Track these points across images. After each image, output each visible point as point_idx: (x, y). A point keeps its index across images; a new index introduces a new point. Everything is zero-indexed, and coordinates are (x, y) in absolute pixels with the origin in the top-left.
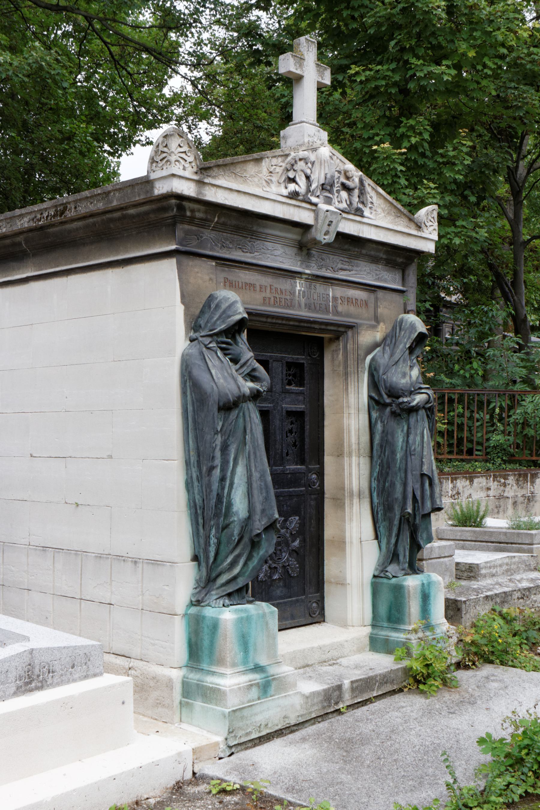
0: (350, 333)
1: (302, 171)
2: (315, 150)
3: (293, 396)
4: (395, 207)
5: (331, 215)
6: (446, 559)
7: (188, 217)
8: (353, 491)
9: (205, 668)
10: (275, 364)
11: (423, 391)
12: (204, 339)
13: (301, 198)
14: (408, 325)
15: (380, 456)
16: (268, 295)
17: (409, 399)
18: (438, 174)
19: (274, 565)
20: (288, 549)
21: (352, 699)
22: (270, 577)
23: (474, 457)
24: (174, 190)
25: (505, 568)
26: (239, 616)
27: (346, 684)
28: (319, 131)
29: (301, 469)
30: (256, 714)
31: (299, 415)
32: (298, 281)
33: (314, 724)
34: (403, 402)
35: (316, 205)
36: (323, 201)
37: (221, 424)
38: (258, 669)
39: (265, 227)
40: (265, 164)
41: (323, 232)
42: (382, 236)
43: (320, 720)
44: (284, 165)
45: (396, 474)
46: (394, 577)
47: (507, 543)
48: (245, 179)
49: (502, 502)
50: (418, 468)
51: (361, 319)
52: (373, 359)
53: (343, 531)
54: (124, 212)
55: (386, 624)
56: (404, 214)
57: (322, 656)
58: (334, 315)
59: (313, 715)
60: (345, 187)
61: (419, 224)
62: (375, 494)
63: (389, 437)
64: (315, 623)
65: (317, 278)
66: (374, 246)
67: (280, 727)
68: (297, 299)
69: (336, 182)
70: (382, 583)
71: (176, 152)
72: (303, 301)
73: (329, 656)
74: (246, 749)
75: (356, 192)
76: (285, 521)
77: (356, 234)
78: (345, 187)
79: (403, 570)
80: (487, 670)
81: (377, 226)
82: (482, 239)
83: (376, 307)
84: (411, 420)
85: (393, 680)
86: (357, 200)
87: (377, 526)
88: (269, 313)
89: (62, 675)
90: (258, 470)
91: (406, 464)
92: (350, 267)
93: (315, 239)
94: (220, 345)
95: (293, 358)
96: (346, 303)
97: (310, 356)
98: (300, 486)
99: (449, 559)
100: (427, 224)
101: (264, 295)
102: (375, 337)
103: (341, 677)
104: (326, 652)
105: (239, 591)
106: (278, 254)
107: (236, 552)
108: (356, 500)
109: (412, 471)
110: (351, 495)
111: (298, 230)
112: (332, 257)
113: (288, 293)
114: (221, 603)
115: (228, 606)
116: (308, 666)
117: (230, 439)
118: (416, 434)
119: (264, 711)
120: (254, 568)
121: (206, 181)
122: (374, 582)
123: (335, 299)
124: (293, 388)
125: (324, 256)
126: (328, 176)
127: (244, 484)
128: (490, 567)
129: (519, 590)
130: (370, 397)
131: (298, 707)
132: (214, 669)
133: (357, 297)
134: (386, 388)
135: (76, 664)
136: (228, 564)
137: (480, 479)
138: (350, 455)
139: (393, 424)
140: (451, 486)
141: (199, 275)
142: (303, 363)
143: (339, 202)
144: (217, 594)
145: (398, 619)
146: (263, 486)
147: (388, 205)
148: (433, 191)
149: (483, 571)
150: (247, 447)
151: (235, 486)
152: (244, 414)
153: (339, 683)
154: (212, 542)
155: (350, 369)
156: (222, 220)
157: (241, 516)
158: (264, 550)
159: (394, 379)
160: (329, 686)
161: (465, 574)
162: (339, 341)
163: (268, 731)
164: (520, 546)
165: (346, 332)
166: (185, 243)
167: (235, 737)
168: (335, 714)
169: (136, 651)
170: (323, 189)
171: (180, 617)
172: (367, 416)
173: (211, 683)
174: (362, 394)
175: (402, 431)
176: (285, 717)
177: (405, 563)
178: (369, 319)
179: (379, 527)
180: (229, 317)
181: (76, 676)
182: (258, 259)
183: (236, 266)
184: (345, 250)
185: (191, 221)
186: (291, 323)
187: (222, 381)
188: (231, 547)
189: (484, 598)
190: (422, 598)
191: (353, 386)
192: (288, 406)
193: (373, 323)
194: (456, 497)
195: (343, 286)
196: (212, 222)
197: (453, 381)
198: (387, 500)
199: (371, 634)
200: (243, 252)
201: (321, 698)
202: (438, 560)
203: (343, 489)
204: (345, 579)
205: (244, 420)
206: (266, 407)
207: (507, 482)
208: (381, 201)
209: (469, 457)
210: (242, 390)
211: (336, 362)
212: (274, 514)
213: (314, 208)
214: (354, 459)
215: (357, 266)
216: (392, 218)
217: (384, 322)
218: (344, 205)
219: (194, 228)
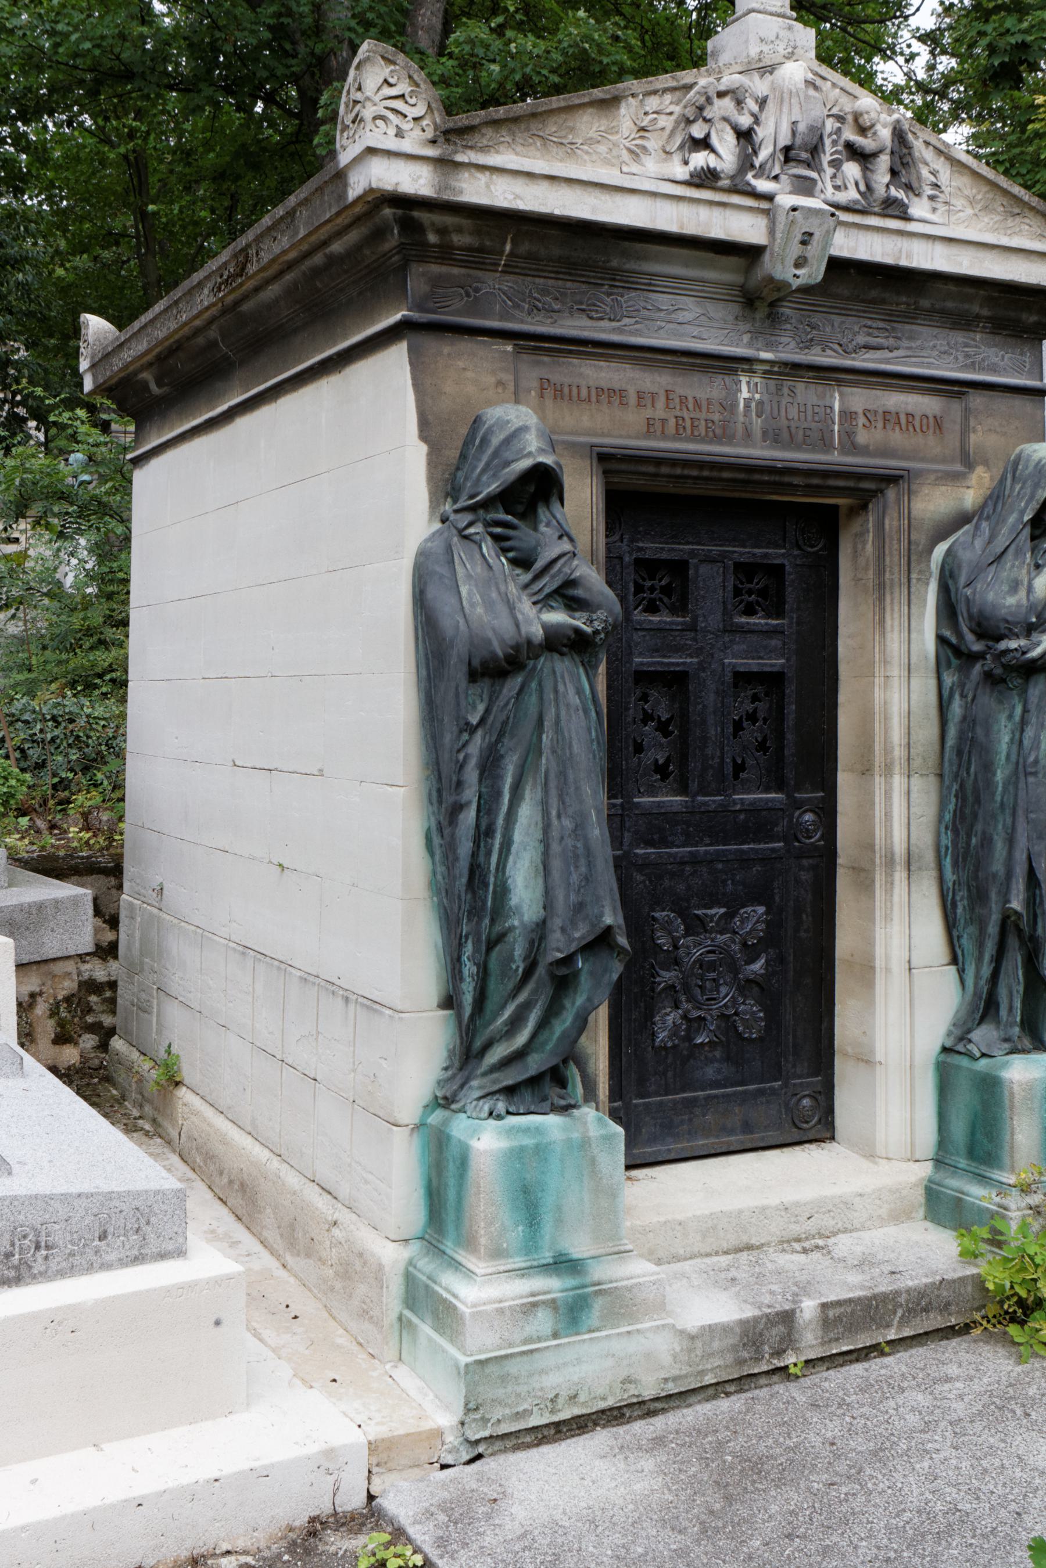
0: (891, 493)
1: (725, 119)
2: (767, 70)
3: (754, 638)
4: (1006, 192)
5: (806, 218)
7: (434, 246)
8: (893, 854)
9: (449, 1251)
10: (704, 569)
12: (459, 516)
13: (724, 183)
14: (1031, 468)
15: (956, 775)
16: (660, 411)
17: (1023, 642)
19: (695, 1014)
20: (735, 977)
21: (823, 1344)
24: (374, 186)
26: (515, 1143)
27: (809, 1308)
28: (790, 28)
30: (543, 1372)
32: (744, 380)
33: (715, 1397)
34: (1008, 651)
35: (769, 198)
36: (788, 188)
37: (481, 708)
38: (564, 1264)
39: (645, 258)
40: (627, 114)
41: (790, 261)
43: (731, 1388)
44: (677, 109)
45: (994, 817)
46: (984, 1055)
48: (570, 150)
51: (923, 460)
52: (949, 552)
53: (870, 942)
54: (327, 251)
55: (963, 1163)
56: (1032, 209)
57: (793, 1226)
58: (843, 451)
59: (709, 1379)
60: (854, 152)
62: (948, 862)
63: (979, 731)
64: (810, 1142)
65: (795, 369)
66: (952, 287)
67: (610, 1402)
68: (741, 419)
69: (828, 142)
70: (958, 1067)
71: (377, 99)
72: (757, 424)
73: (811, 1226)
74: (516, 1448)
75: (884, 161)
76: (730, 916)
77: (889, 260)
78: (854, 152)
79: (1006, 1040)
83: (965, 431)
84: (1031, 691)
86: (887, 178)
87: (955, 933)
89: (72, 1254)
90: (570, 811)
91: (1016, 795)
92: (891, 341)
93: (771, 279)
94: (491, 529)
96: (880, 425)
97: (800, 548)
98: (772, 839)
101: (649, 413)
102: (961, 500)
103: (805, 1289)
105: (534, 1082)
106: (693, 322)
107: (522, 998)
108: (900, 875)
109: (1027, 811)
110: (890, 862)
111: (733, 260)
112: (837, 320)
114: (486, 1108)
115: (499, 1117)
116: (749, 1248)
117: (506, 741)
119: (565, 1364)
120: (564, 1035)
121: (460, 158)
122: (944, 1062)
123: (848, 415)
124: (757, 621)
125: (816, 319)
126: (802, 127)
127: (537, 844)
130: (941, 639)
131: (666, 1359)
132: (461, 1256)
133: (910, 409)
134: (971, 617)
135: (111, 1230)
136: (505, 1023)
139: (987, 700)
141: (469, 374)
142: (783, 566)
143: (837, 188)
144: (480, 1088)
145: (990, 1155)
146: (581, 851)
147: (985, 188)
150: (544, 761)
151: (514, 848)
152: (540, 684)
154: (466, 972)
155: (894, 574)
156: (525, 248)
157: (526, 918)
158: (584, 997)
159: (991, 596)
160: (757, 1313)
163: (577, 1411)
165: (882, 491)
166: (431, 305)
167: (485, 1420)
168: (775, 1378)
169: (344, 1191)
170: (787, 160)
171: (406, 1131)
172: (932, 683)
173: (446, 1289)
174: (921, 632)
175: (1010, 717)
176: (628, 1380)
177: (1012, 1025)
178: (944, 460)
179: (959, 937)
180: (507, 463)
181: (112, 1257)
182: (631, 333)
183: (571, 352)
184: (873, 301)
185: (445, 253)
186: (726, 475)
187: (480, 610)
188: (510, 986)
191: (896, 615)
192: (739, 659)
193: (958, 467)
196: (501, 253)
199: (930, 1181)
200: (591, 318)
201: (731, 1341)
203: (872, 847)
204: (872, 1051)
205: (541, 699)
206: (678, 664)
208: (964, 181)
210: (523, 630)
211: (862, 561)
212: (602, 915)
213: (764, 205)
214: (898, 781)
215: (911, 338)
216: (997, 218)
218: (851, 195)
219: (456, 271)
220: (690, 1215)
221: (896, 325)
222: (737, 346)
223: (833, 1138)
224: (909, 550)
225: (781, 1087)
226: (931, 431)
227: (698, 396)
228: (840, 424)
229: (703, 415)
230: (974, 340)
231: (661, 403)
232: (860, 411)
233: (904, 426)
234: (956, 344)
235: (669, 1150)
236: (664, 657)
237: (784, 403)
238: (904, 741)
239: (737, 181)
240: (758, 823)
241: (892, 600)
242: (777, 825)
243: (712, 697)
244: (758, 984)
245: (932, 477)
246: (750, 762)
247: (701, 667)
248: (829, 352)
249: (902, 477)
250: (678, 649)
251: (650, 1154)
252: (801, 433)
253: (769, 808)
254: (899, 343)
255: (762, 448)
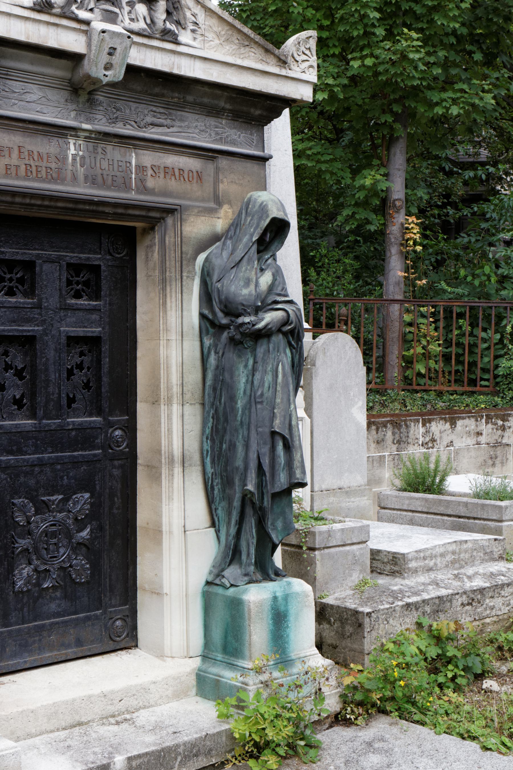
0: (170, 220)
3: (81, 314)
4: (239, 31)
5: (111, 38)
6: (355, 547)
8: (173, 456)
10: (46, 267)
11: (279, 306)
13: (57, 11)
14: (257, 207)
15: (213, 404)
16: (14, 160)
17: (253, 318)
18: (428, 22)
19: (42, 568)
20: (70, 542)
22: (38, 584)
23: (478, 388)
25: (449, 558)
29: (94, 421)
31: (93, 342)
32: (72, 142)
34: (243, 324)
35: (87, 23)
36: (100, 18)
42: (215, 74)
45: (237, 430)
46: (232, 585)
47: (469, 518)
49: (499, 451)
50: (267, 423)
51: (190, 199)
52: (207, 260)
53: (159, 515)
56: (256, 43)
57: (109, 707)
58: (138, 191)
61: (283, 58)
62: (208, 460)
63: (227, 375)
64: (121, 649)
65: (106, 136)
66: (206, 89)
68: (70, 168)
70: (217, 594)
72: (81, 171)
73: (121, 706)
76: (65, 500)
77: (166, 69)
79: (246, 575)
80: (381, 727)
81: (205, 59)
82: (490, 107)
83: (216, 182)
84: (258, 350)
85: (210, 750)
86: (164, 16)
87: (213, 507)
88: (47, 193)
92: (169, 122)
95: (80, 258)
96: (162, 175)
97: (111, 255)
98: (94, 448)
99: (361, 546)
100: (298, 58)
102: (214, 226)
104: (116, 702)
108: (178, 470)
109: (257, 427)
110: (171, 461)
112: (134, 105)
113: (53, 159)
116: (80, 724)
118: (265, 372)
122: (207, 591)
123: (141, 168)
124: (83, 302)
125: (120, 104)
128: (425, 558)
129: (465, 593)
130: (202, 316)
133: (181, 166)
134: (221, 301)
137: (467, 421)
138: (169, 402)
139: (231, 355)
140: (422, 430)
142: (100, 266)
145: (236, 649)
147: (227, 28)
148: (415, 43)
149: (413, 565)
153: (105, 762)
155: (172, 273)
159: (233, 288)
161: (388, 568)
162: (154, 232)
164: (485, 522)
165: (163, 219)
172: (197, 344)
174: (190, 311)
175: (246, 366)
177: (249, 565)
184: (157, 95)
189: (402, 606)
190: (273, 619)
191: (174, 300)
193: (212, 205)
194: (430, 445)
195: (155, 150)
197: (459, 290)
198: (226, 470)
199: (199, 670)
202: (341, 549)
203: (159, 452)
204: (161, 587)
206: (29, 331)
207: (507, 424)
208: (213, 22)
209: (471, 389)
211: (151, 264)
213: (84, 27)
214: (176, 408)
215: (181, 120)
216: (235, 47)
217: (230, 203)
218: (141, 25)
220: (39, 705)
221: (171, 111)
222: (67, 119)
223: (136, 646)
224: (182, 257)
225: (102, 614)
226: (195, 180)
227: (41, 151)
228: (136, 174)
229: (44, 164)
230: (221, 124)
231: (15, 154)
232: (149, 166)
233: (177, 177)
234: (210, 126)
235: (25, 662)
236: (19, 326)
237: (98, 158)
238: (179, 382)
239: (65, 10)
240: (85, 437)
241: (171, 289)
242: (97, 438)
243: (52, 353)
244: (85, 545)
245: (196, 211)
246: (79, 396)
247: (45, 332)
248: (128, 126)
249: (176, 210)
250: (29, 321)
251: (12, 665)
252: (110, 178)
253: (92, 427)
254: (174, 123)
255: (85, 187)
